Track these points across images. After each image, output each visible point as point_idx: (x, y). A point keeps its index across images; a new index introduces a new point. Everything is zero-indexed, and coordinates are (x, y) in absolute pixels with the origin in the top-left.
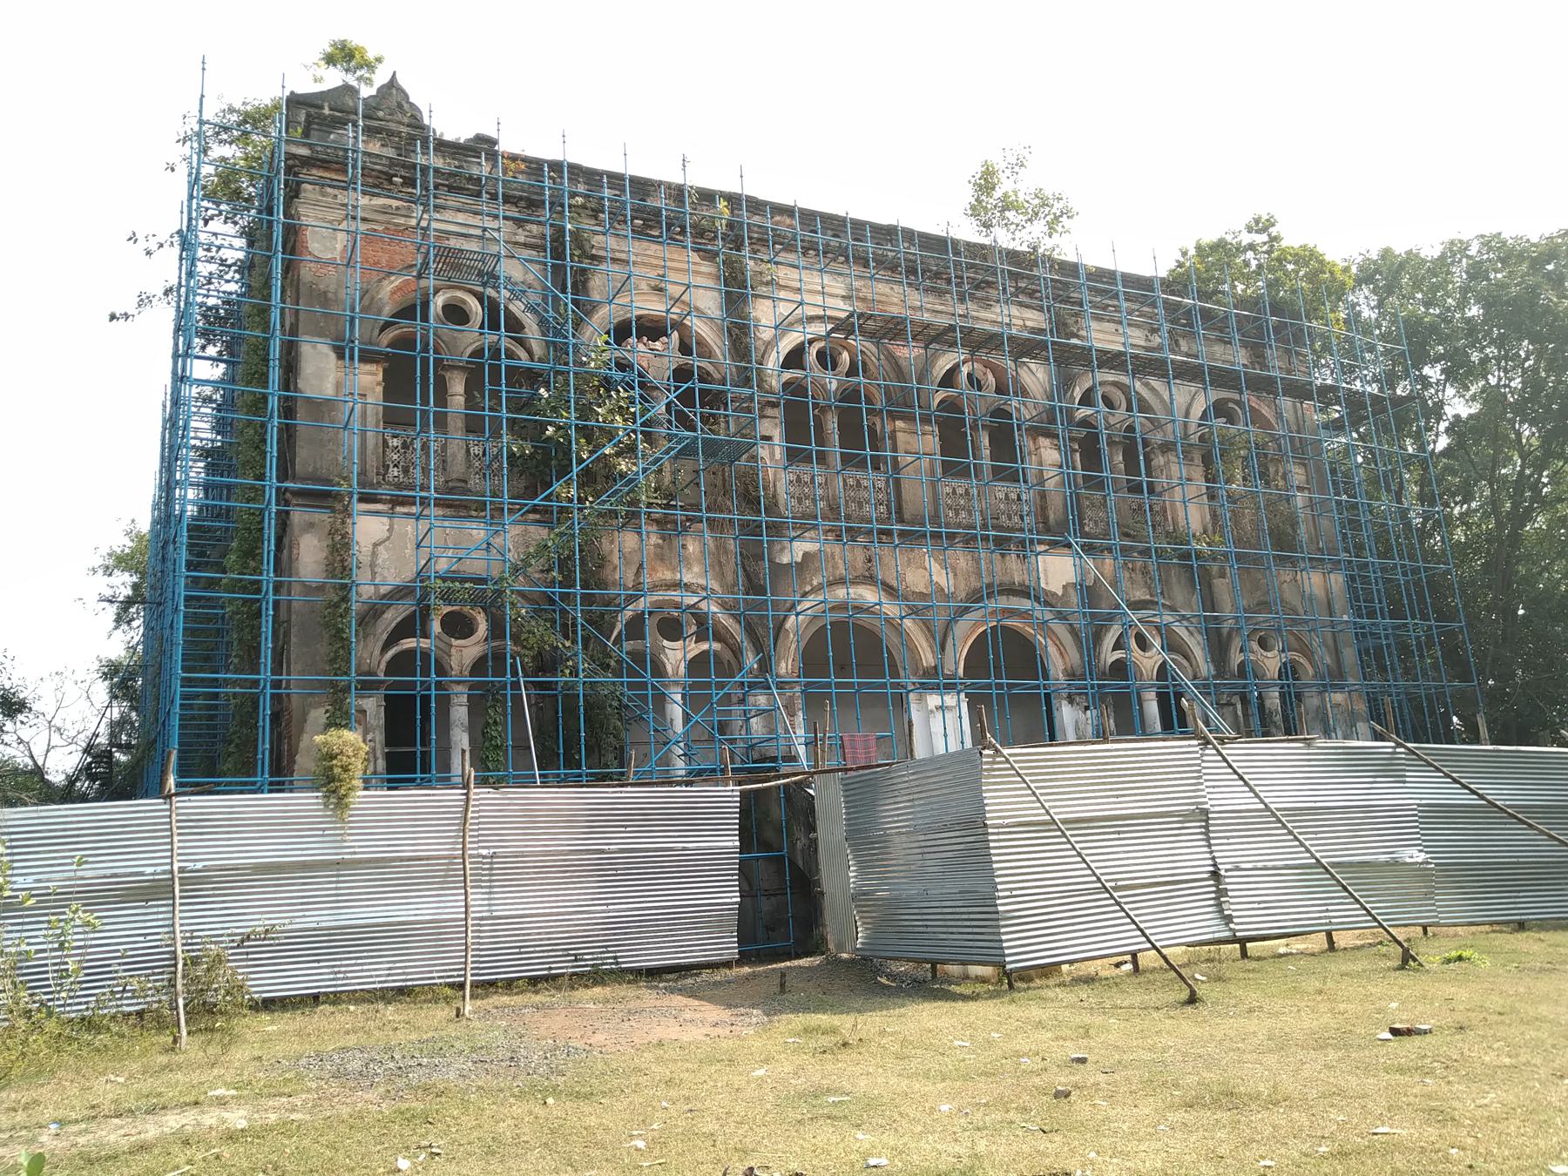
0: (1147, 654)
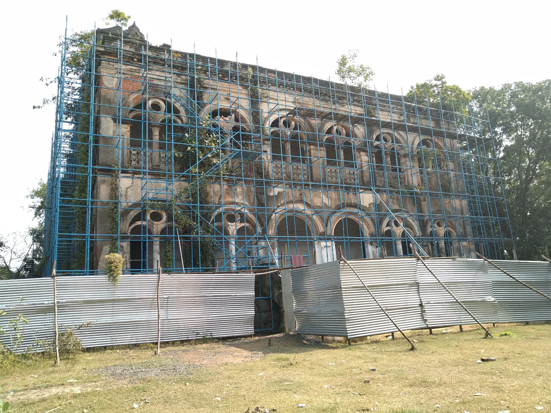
0: (398, 228)
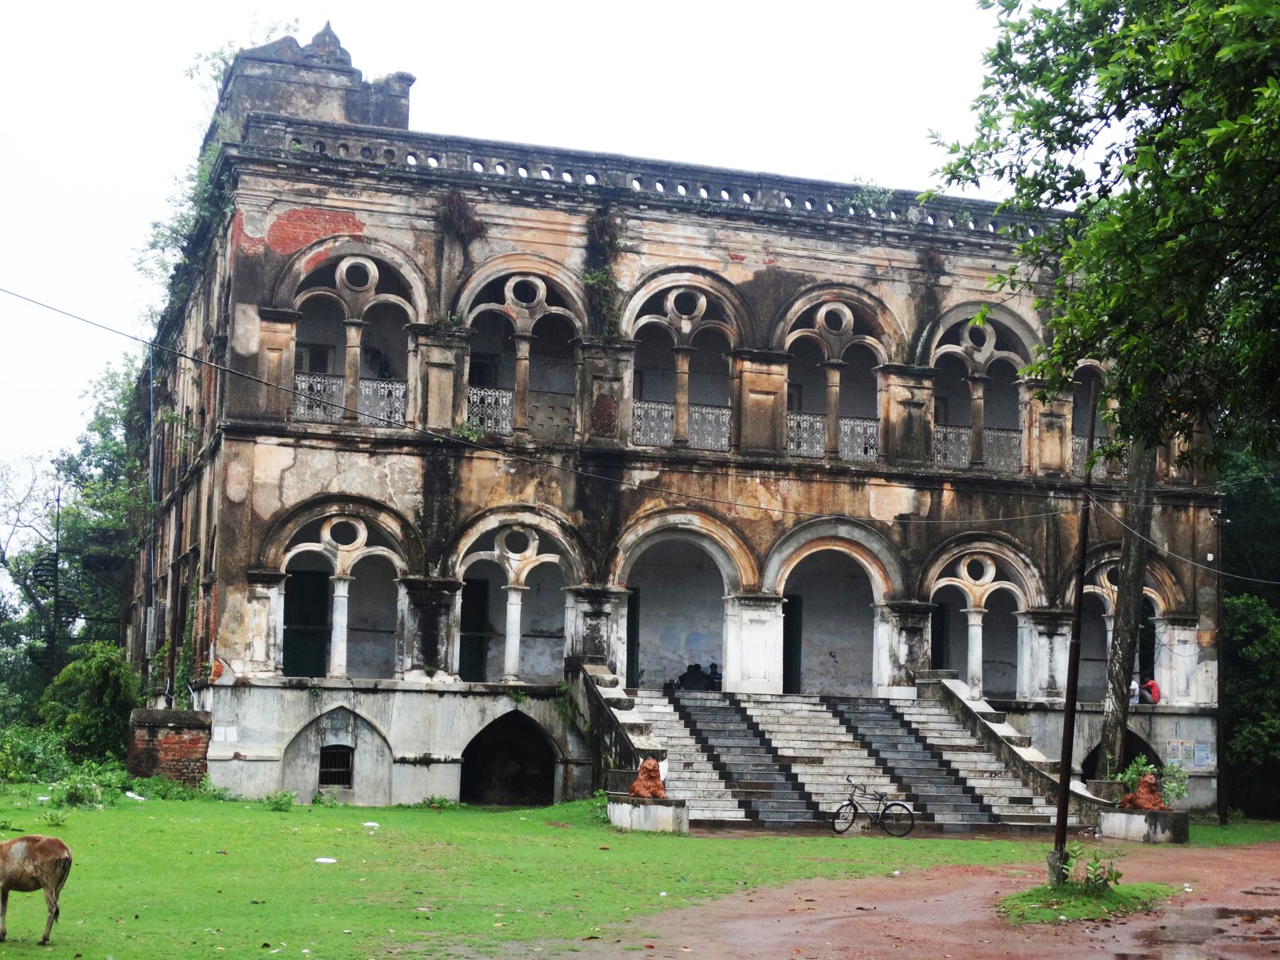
0: (978, 582)
